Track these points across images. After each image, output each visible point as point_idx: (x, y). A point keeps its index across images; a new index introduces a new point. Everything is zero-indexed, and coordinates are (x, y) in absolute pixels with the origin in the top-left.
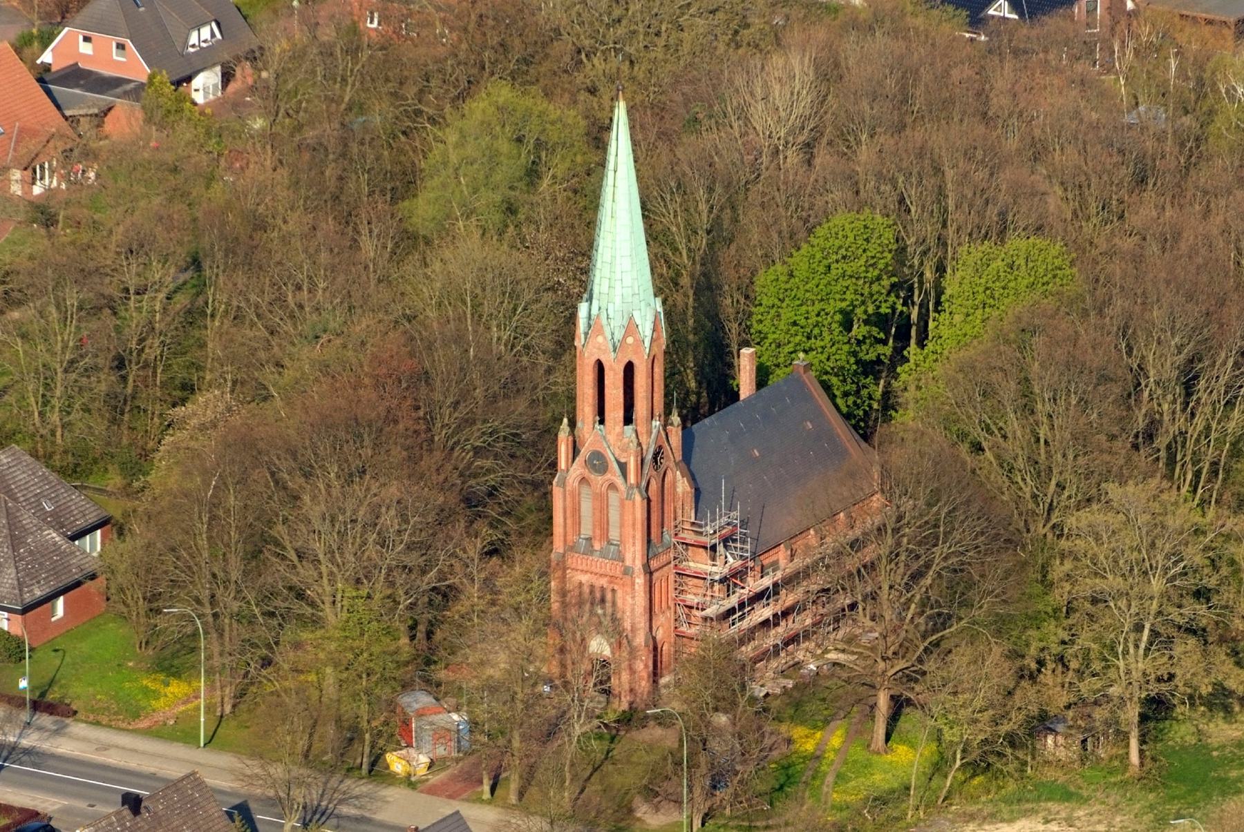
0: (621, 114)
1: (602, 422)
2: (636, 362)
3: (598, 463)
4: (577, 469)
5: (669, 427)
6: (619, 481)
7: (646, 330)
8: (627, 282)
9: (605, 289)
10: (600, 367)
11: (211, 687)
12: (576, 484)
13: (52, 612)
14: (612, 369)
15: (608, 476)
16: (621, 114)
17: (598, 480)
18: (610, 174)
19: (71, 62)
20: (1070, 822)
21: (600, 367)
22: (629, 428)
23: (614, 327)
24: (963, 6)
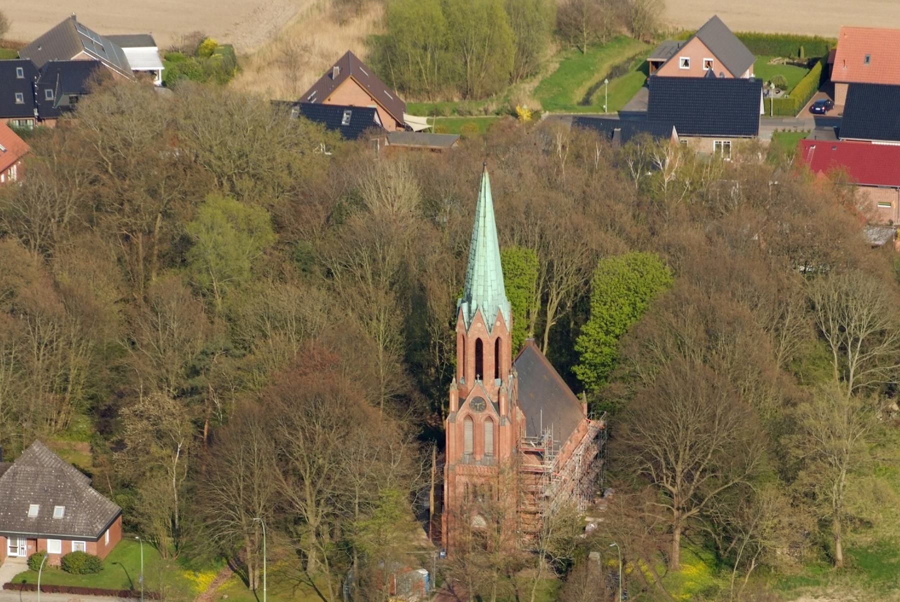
0: (486, 180)
1: (481, 378)
2: (502, 337)
3: (479, 403)
4: (465, 409)
5: (495, 401)
6: (494, 415)
7: (507, 315)
8: (495, 287)
9: (481, 292)
10: (479, 343)
11: (762, 154)
12: (462, 420)
13: (104, 541)
14: (488, 343)
15: (487, 412)
16: (486, 180)
17: (480, 416)
18: (481, 219)
19: (711, 16)
20: (826, 595)
21: (479, 343)
22: (499, 380)
23: (488, 316)
24: (720, 79)
